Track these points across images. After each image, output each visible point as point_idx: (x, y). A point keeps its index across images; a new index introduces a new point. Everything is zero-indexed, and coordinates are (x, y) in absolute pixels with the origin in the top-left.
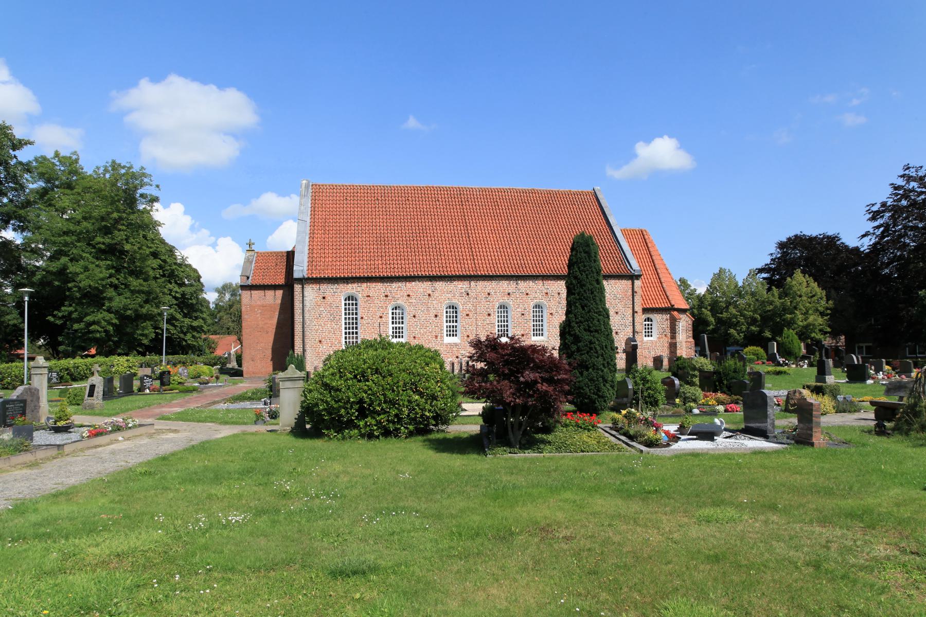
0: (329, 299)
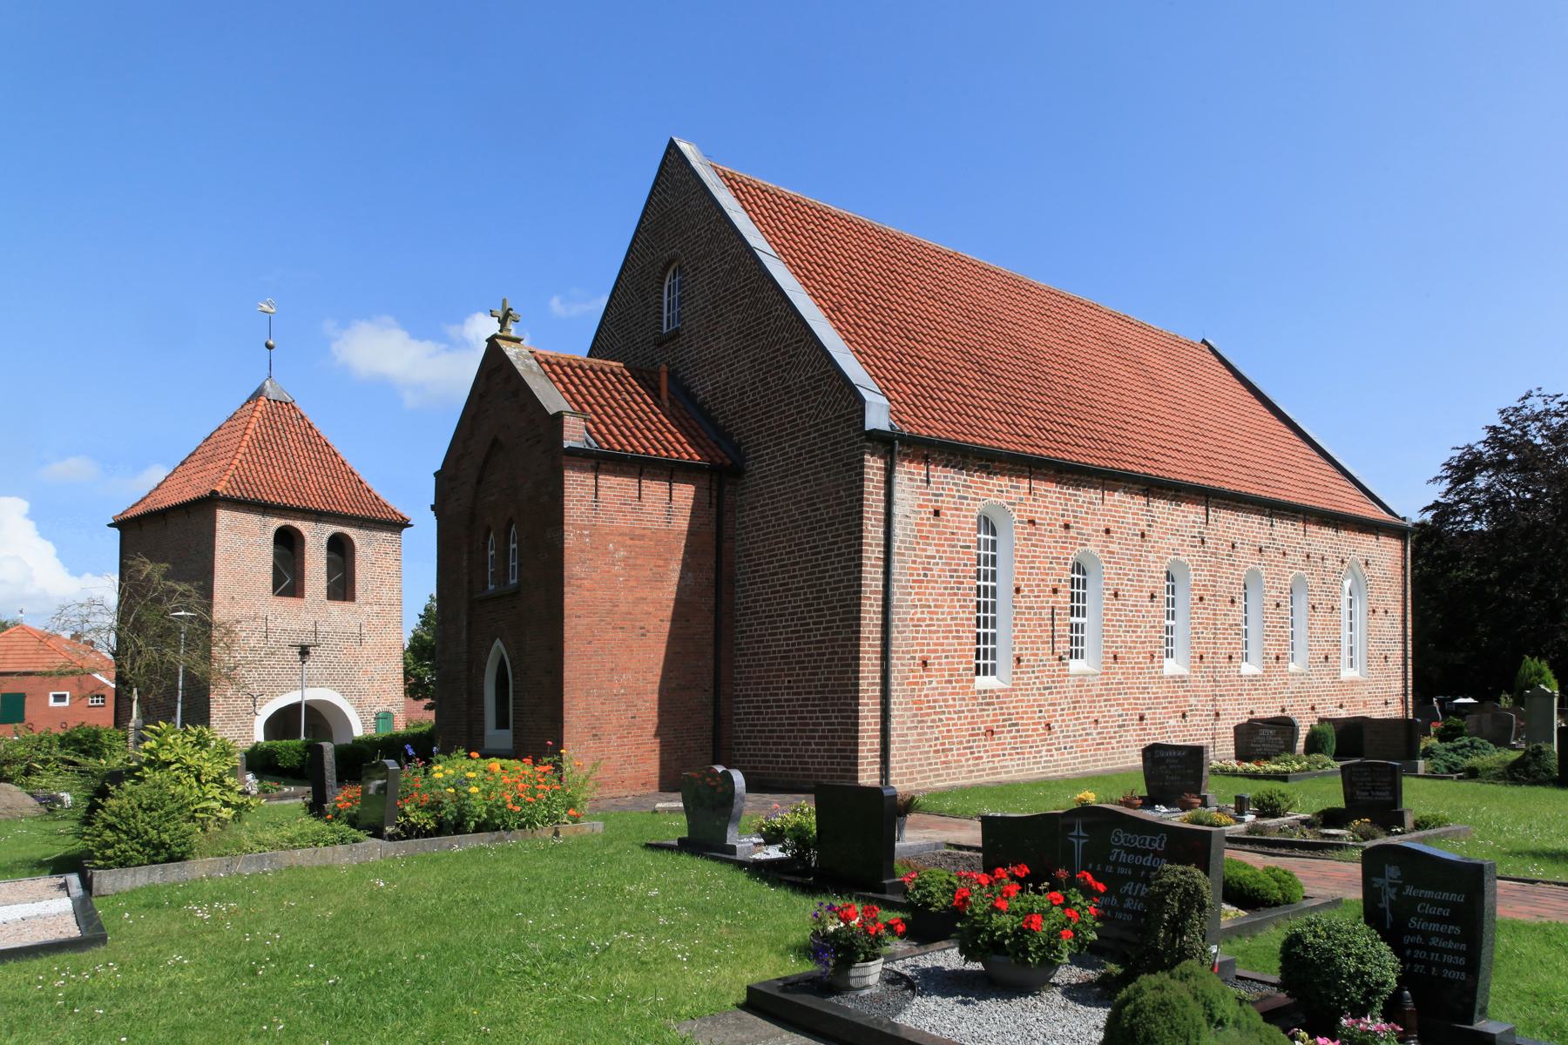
0: (947, 514)
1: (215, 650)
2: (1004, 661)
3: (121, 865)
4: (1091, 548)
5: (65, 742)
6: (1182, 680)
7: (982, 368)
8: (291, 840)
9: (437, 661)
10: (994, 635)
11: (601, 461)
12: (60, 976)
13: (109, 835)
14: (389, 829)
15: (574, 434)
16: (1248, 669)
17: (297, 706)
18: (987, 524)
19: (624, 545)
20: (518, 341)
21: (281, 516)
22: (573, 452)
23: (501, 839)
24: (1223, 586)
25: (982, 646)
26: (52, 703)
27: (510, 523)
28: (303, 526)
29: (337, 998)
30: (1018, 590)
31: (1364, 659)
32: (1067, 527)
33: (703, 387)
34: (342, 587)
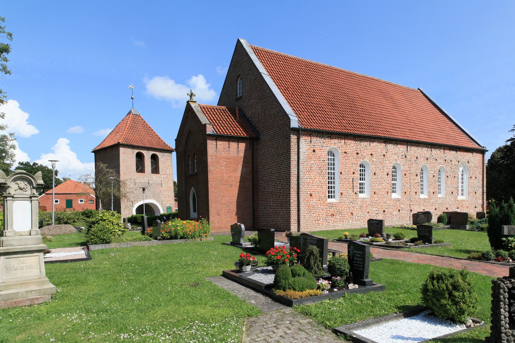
0: (317, 151)
1: (121, 189)
2: (337, 194)
3: (95, 244)
4: (366, 160)
5: (83, 214)
6: (399, 200)
7: (333, 105)
8: (134, 240)
9: (181, 192)
10: (334, 187)
11: (217, 137)
12: (82, 265)
13: (92, 237)
14: (159, 238)
15: (210, 130)
16: (422, 196)
17: (143, 205)
18: (331, 153)
19: (226, 162)
20: (195, 102)
21: (137, 149)
22: (209, 135)
23: (187, 241)
24: (413, 171)
25: (330, 190)
26: (79, 202)
27: (195, 154)
28: (144, 152)
29: (137, 271)
30: (341, 173)
31: (467, 193)
32: (357, 154)
33: (248, 114)
34: (155, 170)
